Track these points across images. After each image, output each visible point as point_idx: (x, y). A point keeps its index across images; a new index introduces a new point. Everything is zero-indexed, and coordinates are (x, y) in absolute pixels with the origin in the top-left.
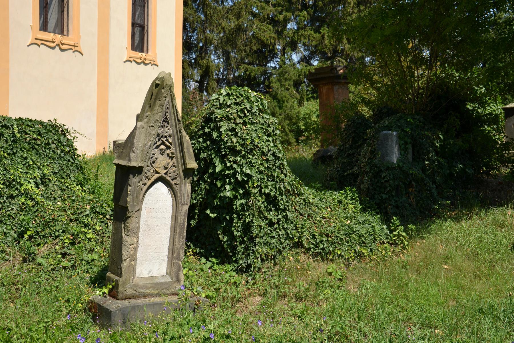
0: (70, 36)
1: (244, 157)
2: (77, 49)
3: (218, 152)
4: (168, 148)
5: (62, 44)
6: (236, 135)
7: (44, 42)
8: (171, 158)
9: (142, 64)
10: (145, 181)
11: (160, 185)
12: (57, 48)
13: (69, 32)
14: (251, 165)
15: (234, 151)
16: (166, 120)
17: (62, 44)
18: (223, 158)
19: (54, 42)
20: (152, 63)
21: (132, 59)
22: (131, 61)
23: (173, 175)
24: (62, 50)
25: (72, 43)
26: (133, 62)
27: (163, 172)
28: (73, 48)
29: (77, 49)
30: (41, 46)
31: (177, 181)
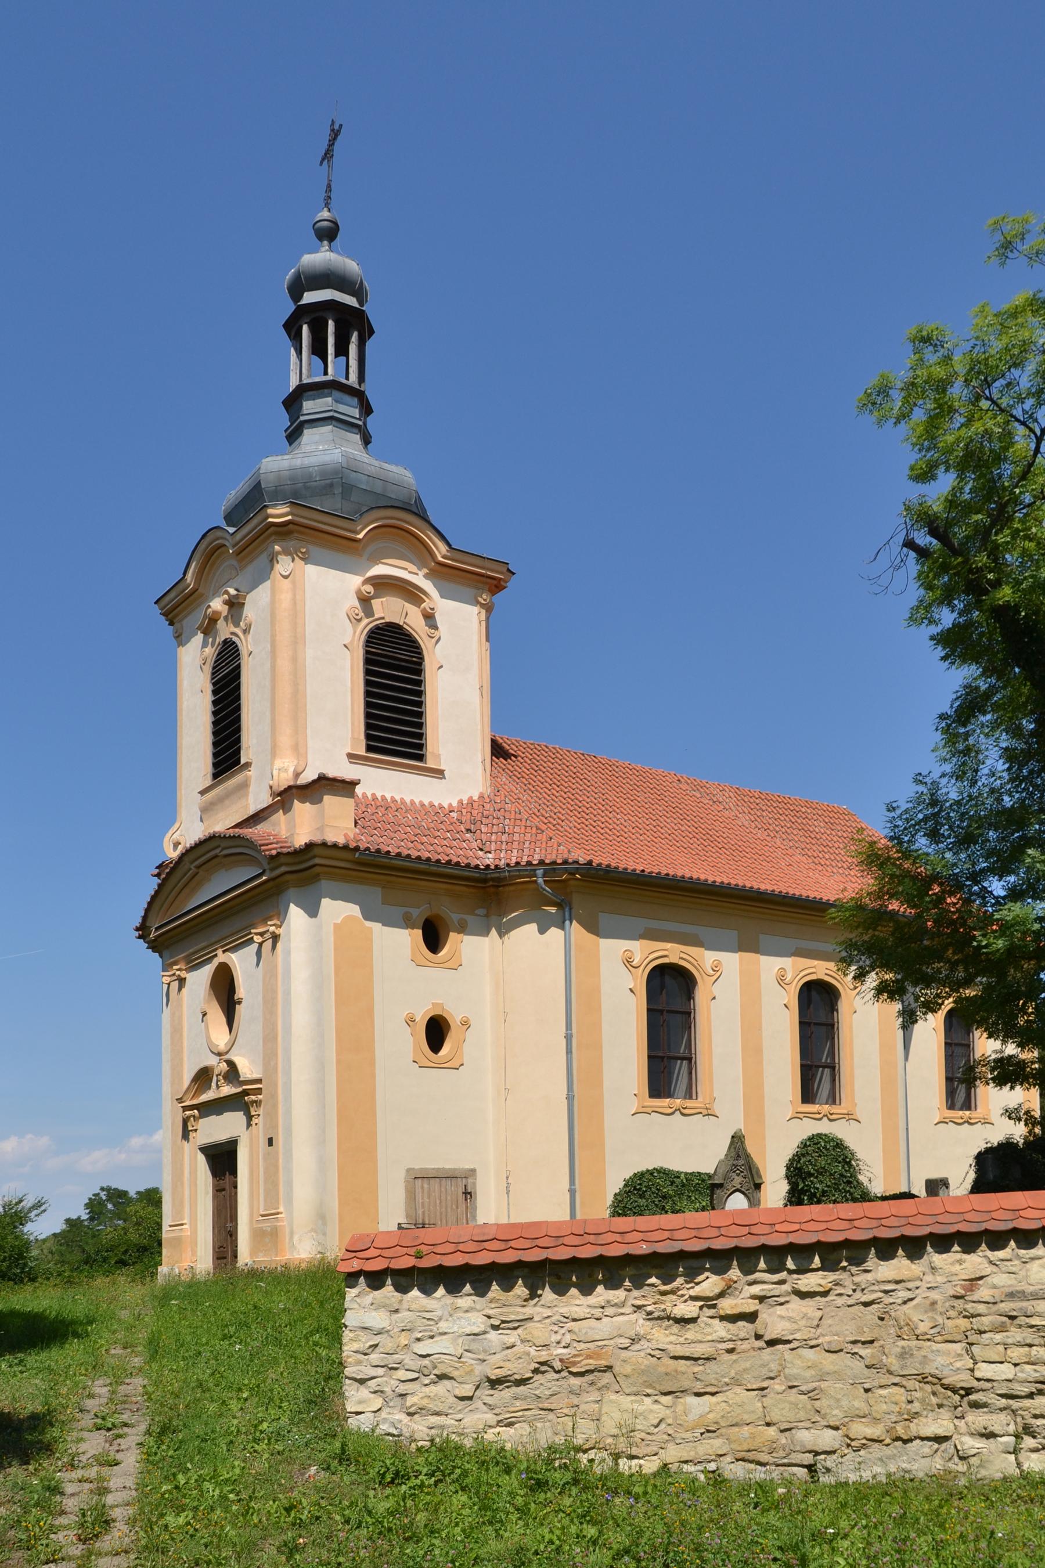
0: (699, 1099)
1: (816, 1177)
2: (851, 1117)
3: (801, 1177)
4: (742, 1172)
5: (831, 1114)
6: (811, 1164)
7: (807, 1115)
8: (745, 1178)
9: (966, 1124)
10: (725, 1191)
11: (737, 1194)
12: (825, 1119)
13: (699, 1095)
14: (821, 1182)
15: (810, 1175)
16: (739, 1156)
17: (831, 1114)
18: (804, 1180)
19: (819, 1113)
20: (983, 1121)
21: (947, 1120)
22: (947, 1123)
23: (747, 1188)
24: (831, 1120)
25: (845, 1112)
26: (950, 1123)
27: (739, 1186)
28: (846, 1116)
29: (851, 1117)
30: (804, 1119)
31: (750, 1191)
